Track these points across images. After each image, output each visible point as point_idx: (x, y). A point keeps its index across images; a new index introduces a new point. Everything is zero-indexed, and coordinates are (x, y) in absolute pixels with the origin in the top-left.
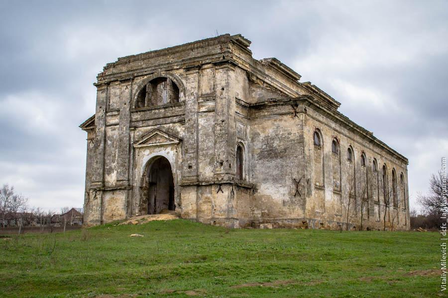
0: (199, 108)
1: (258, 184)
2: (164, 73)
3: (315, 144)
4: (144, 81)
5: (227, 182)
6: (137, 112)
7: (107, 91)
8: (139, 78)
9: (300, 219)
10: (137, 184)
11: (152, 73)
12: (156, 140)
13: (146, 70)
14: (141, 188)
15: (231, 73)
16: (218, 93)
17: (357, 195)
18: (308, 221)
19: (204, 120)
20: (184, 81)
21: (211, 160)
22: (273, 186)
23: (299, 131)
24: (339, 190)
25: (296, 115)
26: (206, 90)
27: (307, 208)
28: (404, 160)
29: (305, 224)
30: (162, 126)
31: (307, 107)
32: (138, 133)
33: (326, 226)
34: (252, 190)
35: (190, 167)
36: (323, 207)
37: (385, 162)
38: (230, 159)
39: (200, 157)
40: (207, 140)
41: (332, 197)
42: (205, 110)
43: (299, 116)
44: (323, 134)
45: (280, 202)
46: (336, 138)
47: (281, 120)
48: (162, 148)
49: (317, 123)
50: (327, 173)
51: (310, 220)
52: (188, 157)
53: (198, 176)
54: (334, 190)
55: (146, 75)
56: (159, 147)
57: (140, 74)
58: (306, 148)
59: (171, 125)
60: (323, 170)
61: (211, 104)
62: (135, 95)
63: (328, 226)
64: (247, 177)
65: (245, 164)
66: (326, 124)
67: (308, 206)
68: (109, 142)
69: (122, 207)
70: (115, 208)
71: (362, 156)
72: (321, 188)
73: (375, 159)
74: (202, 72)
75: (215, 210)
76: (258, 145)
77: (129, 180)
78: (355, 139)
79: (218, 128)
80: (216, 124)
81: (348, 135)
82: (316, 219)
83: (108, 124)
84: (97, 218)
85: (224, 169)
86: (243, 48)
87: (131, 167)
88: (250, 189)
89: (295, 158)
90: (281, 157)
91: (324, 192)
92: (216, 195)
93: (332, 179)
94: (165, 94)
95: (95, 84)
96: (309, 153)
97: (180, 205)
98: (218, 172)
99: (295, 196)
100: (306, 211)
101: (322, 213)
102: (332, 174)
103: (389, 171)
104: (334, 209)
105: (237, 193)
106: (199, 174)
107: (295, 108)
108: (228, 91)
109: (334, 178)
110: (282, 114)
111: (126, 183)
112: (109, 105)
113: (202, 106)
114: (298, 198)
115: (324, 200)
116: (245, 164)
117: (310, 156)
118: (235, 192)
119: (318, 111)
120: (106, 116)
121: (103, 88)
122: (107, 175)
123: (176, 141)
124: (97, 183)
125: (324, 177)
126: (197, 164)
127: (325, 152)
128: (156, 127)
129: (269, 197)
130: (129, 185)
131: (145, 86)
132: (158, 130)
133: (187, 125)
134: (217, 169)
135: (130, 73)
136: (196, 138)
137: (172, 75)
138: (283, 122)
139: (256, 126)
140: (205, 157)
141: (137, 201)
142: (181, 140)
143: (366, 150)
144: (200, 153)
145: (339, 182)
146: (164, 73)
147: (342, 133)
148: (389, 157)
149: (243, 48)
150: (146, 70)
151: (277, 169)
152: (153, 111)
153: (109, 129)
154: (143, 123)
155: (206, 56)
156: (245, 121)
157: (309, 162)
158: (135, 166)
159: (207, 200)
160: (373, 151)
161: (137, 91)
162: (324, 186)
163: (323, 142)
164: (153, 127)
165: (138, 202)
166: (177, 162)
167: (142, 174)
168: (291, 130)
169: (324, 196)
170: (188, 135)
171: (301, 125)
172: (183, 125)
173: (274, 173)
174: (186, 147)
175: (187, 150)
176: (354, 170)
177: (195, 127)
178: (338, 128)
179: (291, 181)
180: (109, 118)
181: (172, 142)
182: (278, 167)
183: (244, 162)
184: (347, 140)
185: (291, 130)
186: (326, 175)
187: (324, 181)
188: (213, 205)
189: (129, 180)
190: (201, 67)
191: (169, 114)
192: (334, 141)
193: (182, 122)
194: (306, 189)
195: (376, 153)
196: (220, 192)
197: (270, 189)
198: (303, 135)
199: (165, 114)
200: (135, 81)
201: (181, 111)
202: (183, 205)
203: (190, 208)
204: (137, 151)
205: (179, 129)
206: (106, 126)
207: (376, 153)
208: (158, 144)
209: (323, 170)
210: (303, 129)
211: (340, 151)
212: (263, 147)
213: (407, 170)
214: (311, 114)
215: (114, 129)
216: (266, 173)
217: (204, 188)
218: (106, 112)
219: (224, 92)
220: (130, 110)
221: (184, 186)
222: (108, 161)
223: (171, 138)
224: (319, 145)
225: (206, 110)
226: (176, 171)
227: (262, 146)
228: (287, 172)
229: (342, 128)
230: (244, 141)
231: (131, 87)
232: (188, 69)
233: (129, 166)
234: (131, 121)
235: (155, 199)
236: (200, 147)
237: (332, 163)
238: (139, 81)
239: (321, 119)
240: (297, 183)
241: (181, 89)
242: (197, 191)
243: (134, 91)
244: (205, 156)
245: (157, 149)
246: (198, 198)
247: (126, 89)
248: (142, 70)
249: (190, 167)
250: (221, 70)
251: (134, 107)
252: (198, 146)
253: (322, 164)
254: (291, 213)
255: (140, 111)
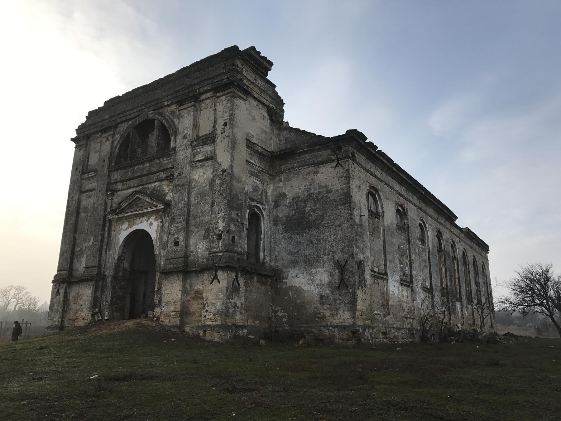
0: (194, 155)
1: (284, 270)
2: (151, 114)
3: (370, 211)
4: (127, 128)
5: (225, 265)
6: (117, 170)
7: (86, 147)
8: (123, 124)
9: (347, 326)
10: (109, 273)
11: (138, 116)
12: (138, 208)
13: (131, 112)
14: (115, 277)
15: (239, 103)
16: (219, 132)
17: (434, 288)
18: (361, 330)
19: (200, 172)
20: (176, 121)
21: (206, 231)
22: (305, 272)
23: (344, 186)
24: (409, 280)
25: (338, 163)
26: (205, 129)
27: (358, 307)
28: (485, 248)
29: (356, 335)
30: (146, 186)
31: (355, 151)
32: (117, 200)
33: (391, 336)
34: (274, 279)
35: (177, 244)
36: (386, 305)
37: (464, 247)
38: (233, 228)
39: (192, 228)
40: (201, 203)
41: (399, 290)
42: (201, 158)
43: (343, 164)
44: (382, 197)
45: (317, 299)
46: (401, 206)
47: (316, 173)
48: (144, 218)
49: (374, 179)
50: (390, 254)
51: (365, 327)
52: (175, 228)
53: (186, 257)
54: (402, 280)
55: (131, 119)
56: (140, 217)
57: (124, 119)
58: (356, 212)
59: (157, 183)
60: (385, 250)
61: (208, 149)
62: (117, 146)
63: (395, 336)
64: (267, 259)
65: (264, 239)
66: (386, 184)
67: (360, 305)
68: (83, 215)
69: (87, 307)
70: (78, 307)
71: (437, 236)
72: (381, 276)
73: (453, 242)
74: (200, 105)
75: (207, 311)
76: (283, 212)
77: (99, 266)
78: (428, 211)
79: (218, 182)
80: (214, 176)
81: (418, 204)
82: (375, 325)
83: (84, 190)
84: (57, 323)
85: (223, 244)
86: (260, 71)
87: (104, 247)
88: (271, 277)
89: (338, 228)
90: (317, 228)
91: (387, 282)
92: (210, 287)
93: (398, 263)
94: (153, 139)
95: (73, 140)
96: (361, 220)
97: (160, 302)
98: (215, 250)
99: (339, 288)
100: (357, 313)
101: (385, 316)
102: (397, 256)
103: (470, 259)
104: (404, 310)
105: (246, 284)
106: (188, 254)
107: (337, 152)
108: (233, 126)
109: (401, 263)
110: (317, 164)
111: (94, 272)
112: (87, 165)
113: (198, 153)
114: (227, 234)
115: (387, 295)
116: (264, 239)
117: (361, 225)
118: (242, 282)
119: (373, 163)
120: (82, 179)
121: (82, 143)
122: (75, 260)
123: (161, 206)
124: (63, 272)
125: (385, 261)
126: (187, 239)
127: (386, 224)
128: (138, 189)
129: (298, 291)
130: (99, 273)
131: (129, 134)
132: (140, 192)
133: (176, 182)
134: (213, 245)
135: (112, 119)
136: (186, 199)
137: (161, 114)
138: (319, 176)
139: (281, 184)
140: (198, 228)
141: (107, 297)
142: (168, 205)
143: (443, 230)
144: (192, 222)
145: (408, 269)
146: (151, 114)
147: (410, 201)
148: (469, 242)
149: (260, 71)
150: (131, 112)
151: (311, 245)
152: (136, 167)
153: (84, 197)
154: (123, 185)
155: (205, 80)
156: (266, 177)
157: (360, 234)
158: (108, 248)
159: (198, 295)
160: (451, 231)
161: (119, 141)
162: (386, 274)
163: (383, 208)
164: (135, 189)
165: (109, 300)
166: (160, 239)
167: (116, 258)
168: (332, 186)
169: (387, 289)
170: (176, 197)
171: (346, 177)
172: (171, 182)
173: (307, 252)
174: (173, 213)
175: (173, 219)
176: (429, 254)
177: (188, 186)
178: (404, 193)
179: (332, 263)
180: (85, 182)
181: (156, 208)
182: (312, 242)
183: (262, 236)
184: (418, 211)
185: (332, 186)
186: (389, 257)
187: (385, 265)
188: (205, 303)
189: (99, 266)
190: (199, 98)
191: (154, 169)
192: (398, 211)
193: (170, 178)
194: (357, 277)
195: (454, 234)
196: (216, 281)
197: (301, 278)
198: (349, 192)
199: (150, 169)
200: (118, 129)
201: (171, 162)
202: (163, 304)
203: (172, 308)
204: (114, 223)
205: (166, 190)
206: (81, 192)
207: (454, 234)
208: (138, 212)
209: (385, 250)
210: (349, 183)
211: (408, 225)
212: (291, 214)
213: (487, 260)
214: (363, 164)
215: (90, 197)
216: (295, 253)
217: (194, 277)
218: (83, 173)
219: (227, 128)
220: (108, 168)
221: (167, 273)
222: (78, 241)
223: (155, 203)
224: (378, 212)
225: (203, 158)
226: (159, 253)
227: (289, 212)
228: (325, 250)
229: (410, 194)
230: (262, 204)
231: (113, 137)
232: (180, 103)
233: (101, 247)
234: (109, 184)
235: (145, 295)
236: (192, 213)
237: (397, 240)
238: (123, 127)
239: (378, 173)
240: (341, 267)
241: (171, 132)
242: (182, 280)
243: (116, 143)
244: (197, 225)
245: (138, 220)
246: (185, 291)
247: (106, 141)
248: (126, 114)
249: (177, 244)
250: (223, 98)
251: (113, 164)
252: (189, 211)
253: (382, 240)
254: (333, 317)
255: (120, 169)
